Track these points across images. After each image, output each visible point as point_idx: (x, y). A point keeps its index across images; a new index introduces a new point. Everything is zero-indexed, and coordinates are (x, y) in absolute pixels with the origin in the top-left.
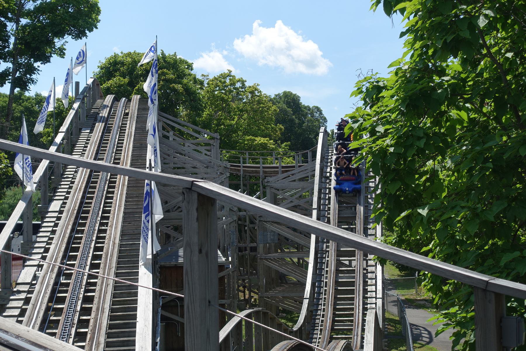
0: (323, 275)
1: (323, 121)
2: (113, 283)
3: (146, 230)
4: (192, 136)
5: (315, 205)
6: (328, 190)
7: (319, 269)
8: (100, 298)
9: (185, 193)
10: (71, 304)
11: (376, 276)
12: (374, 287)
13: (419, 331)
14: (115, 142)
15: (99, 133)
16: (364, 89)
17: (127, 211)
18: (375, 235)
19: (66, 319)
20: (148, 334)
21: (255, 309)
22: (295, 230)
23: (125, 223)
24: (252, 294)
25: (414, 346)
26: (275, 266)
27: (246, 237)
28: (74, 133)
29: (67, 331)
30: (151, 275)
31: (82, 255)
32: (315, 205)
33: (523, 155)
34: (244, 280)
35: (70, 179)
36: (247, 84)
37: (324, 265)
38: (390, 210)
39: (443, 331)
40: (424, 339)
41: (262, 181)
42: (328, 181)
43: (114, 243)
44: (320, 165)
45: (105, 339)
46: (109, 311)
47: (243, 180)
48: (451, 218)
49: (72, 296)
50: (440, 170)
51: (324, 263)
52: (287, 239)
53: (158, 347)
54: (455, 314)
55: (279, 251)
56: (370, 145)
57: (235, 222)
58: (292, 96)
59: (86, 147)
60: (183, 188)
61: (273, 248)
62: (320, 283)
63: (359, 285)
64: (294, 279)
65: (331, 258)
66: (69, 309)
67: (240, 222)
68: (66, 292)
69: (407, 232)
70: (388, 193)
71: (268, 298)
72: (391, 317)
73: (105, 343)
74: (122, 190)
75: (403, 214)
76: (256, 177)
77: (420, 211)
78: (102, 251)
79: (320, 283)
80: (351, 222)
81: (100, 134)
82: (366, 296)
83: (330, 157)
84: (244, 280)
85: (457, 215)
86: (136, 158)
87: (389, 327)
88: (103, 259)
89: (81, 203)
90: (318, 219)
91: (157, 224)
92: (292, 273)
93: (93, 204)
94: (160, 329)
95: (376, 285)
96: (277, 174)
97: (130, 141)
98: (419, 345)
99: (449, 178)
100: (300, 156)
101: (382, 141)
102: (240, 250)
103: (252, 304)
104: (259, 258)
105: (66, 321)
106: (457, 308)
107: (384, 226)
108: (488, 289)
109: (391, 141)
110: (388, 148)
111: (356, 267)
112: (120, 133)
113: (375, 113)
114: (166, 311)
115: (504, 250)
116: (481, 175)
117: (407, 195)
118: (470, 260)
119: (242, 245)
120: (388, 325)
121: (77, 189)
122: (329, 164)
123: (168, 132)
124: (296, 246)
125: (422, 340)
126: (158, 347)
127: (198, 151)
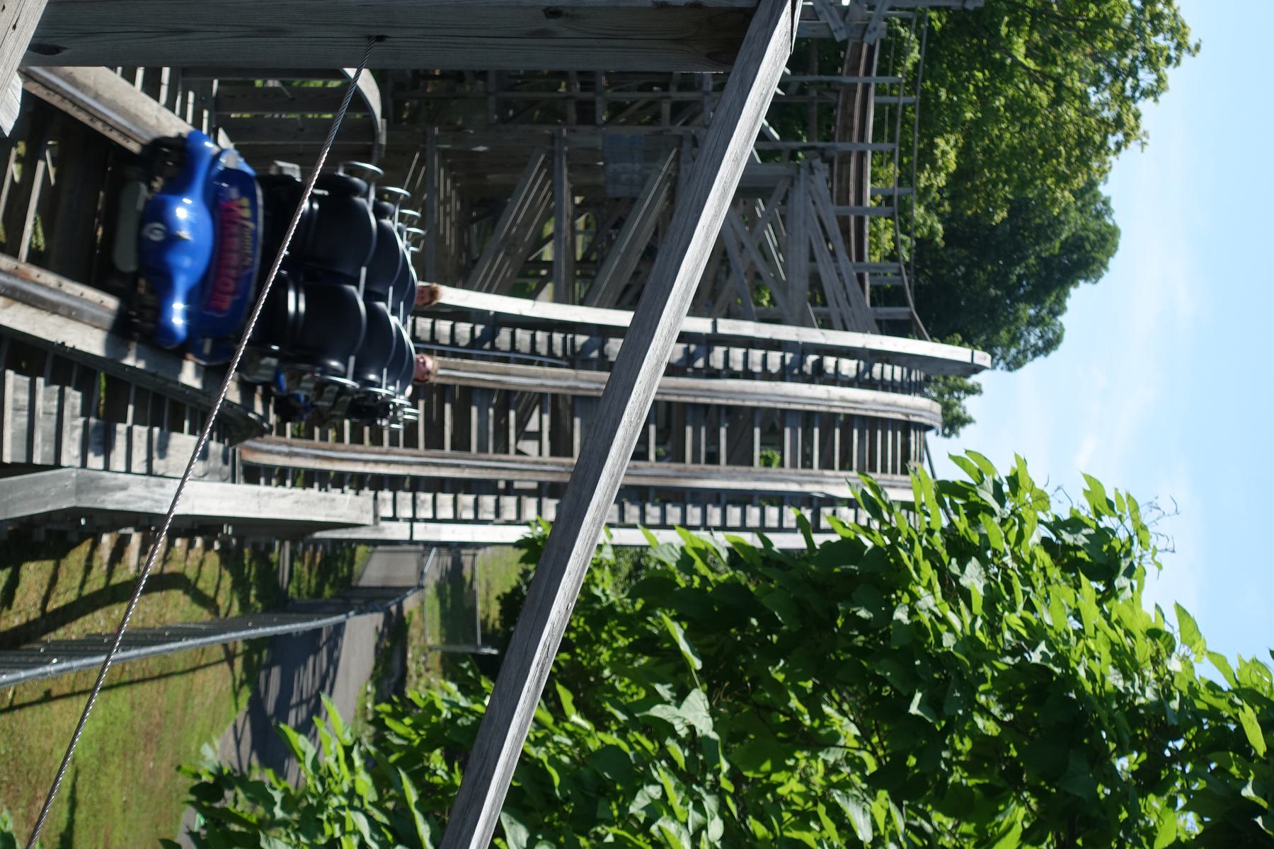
1: (1009, 359)
5: (727, 327)
16: (1107, 522)
18: (622, 524)
22: (650, 254)
32: (727, 327)
36: (1144, 105)
47: (821, 82)
52: (619, 224)
55: (578, 200)
58: (1099, 256)
63: (458, 466)
90: (684, 337)
95: (456, 520)
96: (838, 198)
101: (930, 581)
113: (1027, 559)
124: (594, 257)
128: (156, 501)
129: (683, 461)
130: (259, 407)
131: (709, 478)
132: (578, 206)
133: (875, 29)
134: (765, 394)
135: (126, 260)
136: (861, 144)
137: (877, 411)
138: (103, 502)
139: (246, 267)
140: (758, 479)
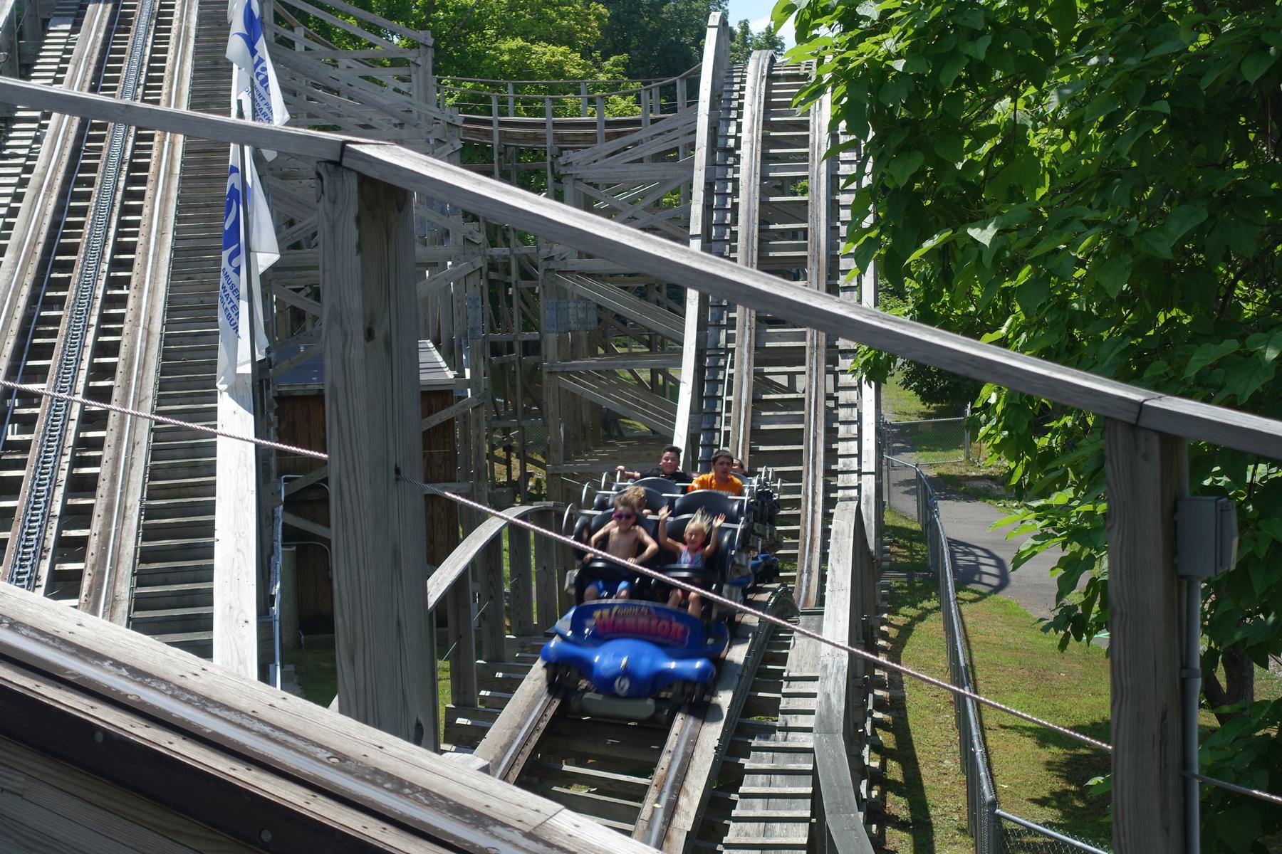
0: (720, 414)
2: (149, 439)
3: (231, 295)
4: (355, 39)
6: (730, 185)
7: (706, 397)
8: (114, 479)
9: (324, 175)
10: (36, 497)
11: (860, 415)
12: (854, 444)
13: (972, 558)
14: (143, 55)
15: (98, 30)
17: (181, 245)
19: (24, 536)
20: (247, 573)
21: (536, 505)
23: (175, 277)
24: (530, 468)
25: (957, 598)
26: (589, 391)
27: (512, 316)
28: (27, 32)
29: (29, 569)
30: (251, 418)
31: (60, 366)
33: (1252, 80)
34: (506, 431)
35: (22, 161)
37: (720, 386)
38: (894, 234)
39: (1035, 553)
40: (986, 579)
41: (552, 164)
42: (731, 160)
43: (148, 333)
44: (710, 116)
45: (131, 589)
46: (140, 515)
47: (499, 160)
48: (1057, 251)
49: (37, 476)
50: (1030, 123)
51: (722, 382)
53: (276, 608)
54: (1065, 509)
55: (601, 351)
56: (840, 53)
57: (478, 273)
59: (64, 71)
60: (318, 162)
61: (584, 344)
62: (710, 435)
63: (815, 438)
64: (643, 427)
65: (740, 370)
66: (29, 512)
67: (493, 275)
68: (21, 465)
69: (940, 295)
70: (890, 185)
71: (573, 477)
72: (901, 523)
73: (131, 598)
74: (167, 189)
75: (928, 244)
76: (535, 152)
77: (974, 233)
78: (116, 355)
79: (710, 435)
80: (794, 271)
81: (101, 35)
82: (833, 467)
83: (736, 95)
84: (506, 431)
85: (1072, 245)
86: (203, 101)
87: (895, 549)
88: (119, 375)
89: (55, 225)
91: (263, 276)
92: (637, 410)
93: (87, 227)
94: (280, 562)
95: (859, 439)
97: (184, 53)
98: (972, 596)
99: (1055, 147)
100: (656, 92)
101: (876, 43)
102: (496, 349)
103: (529, 493)
104: (545, 370)
105: (23, 543)
106: (1069, 493)
107: (880, 282)
108: (1143, 423)
109: (897, 42)
110: (888, 62)
111: (807, 391)
112: (157, 31)
114: (298, 514)
115: (1197, 337)
116: (1140, 134)
117: (942, 192)
118: (1106, 364)
119: (498, 336)
120: (890, 544)
121: (42, 186)
122: (734, 114)
123: (291, 28)
124: (647, 337)
125: (979, 582)
126: (276, 608)
127: (374, 81)
128: (838, 671)
129: (806, 257)
130: (764, 597)
131: (819, 236)
132: (606, 351)
133: (451, 117)
134: (749, 194)
135: (647, 707)
136: (547, 126)
137: (760, 102)
138: (839, 712)
139: (649, 612)
140: (818, 196)
